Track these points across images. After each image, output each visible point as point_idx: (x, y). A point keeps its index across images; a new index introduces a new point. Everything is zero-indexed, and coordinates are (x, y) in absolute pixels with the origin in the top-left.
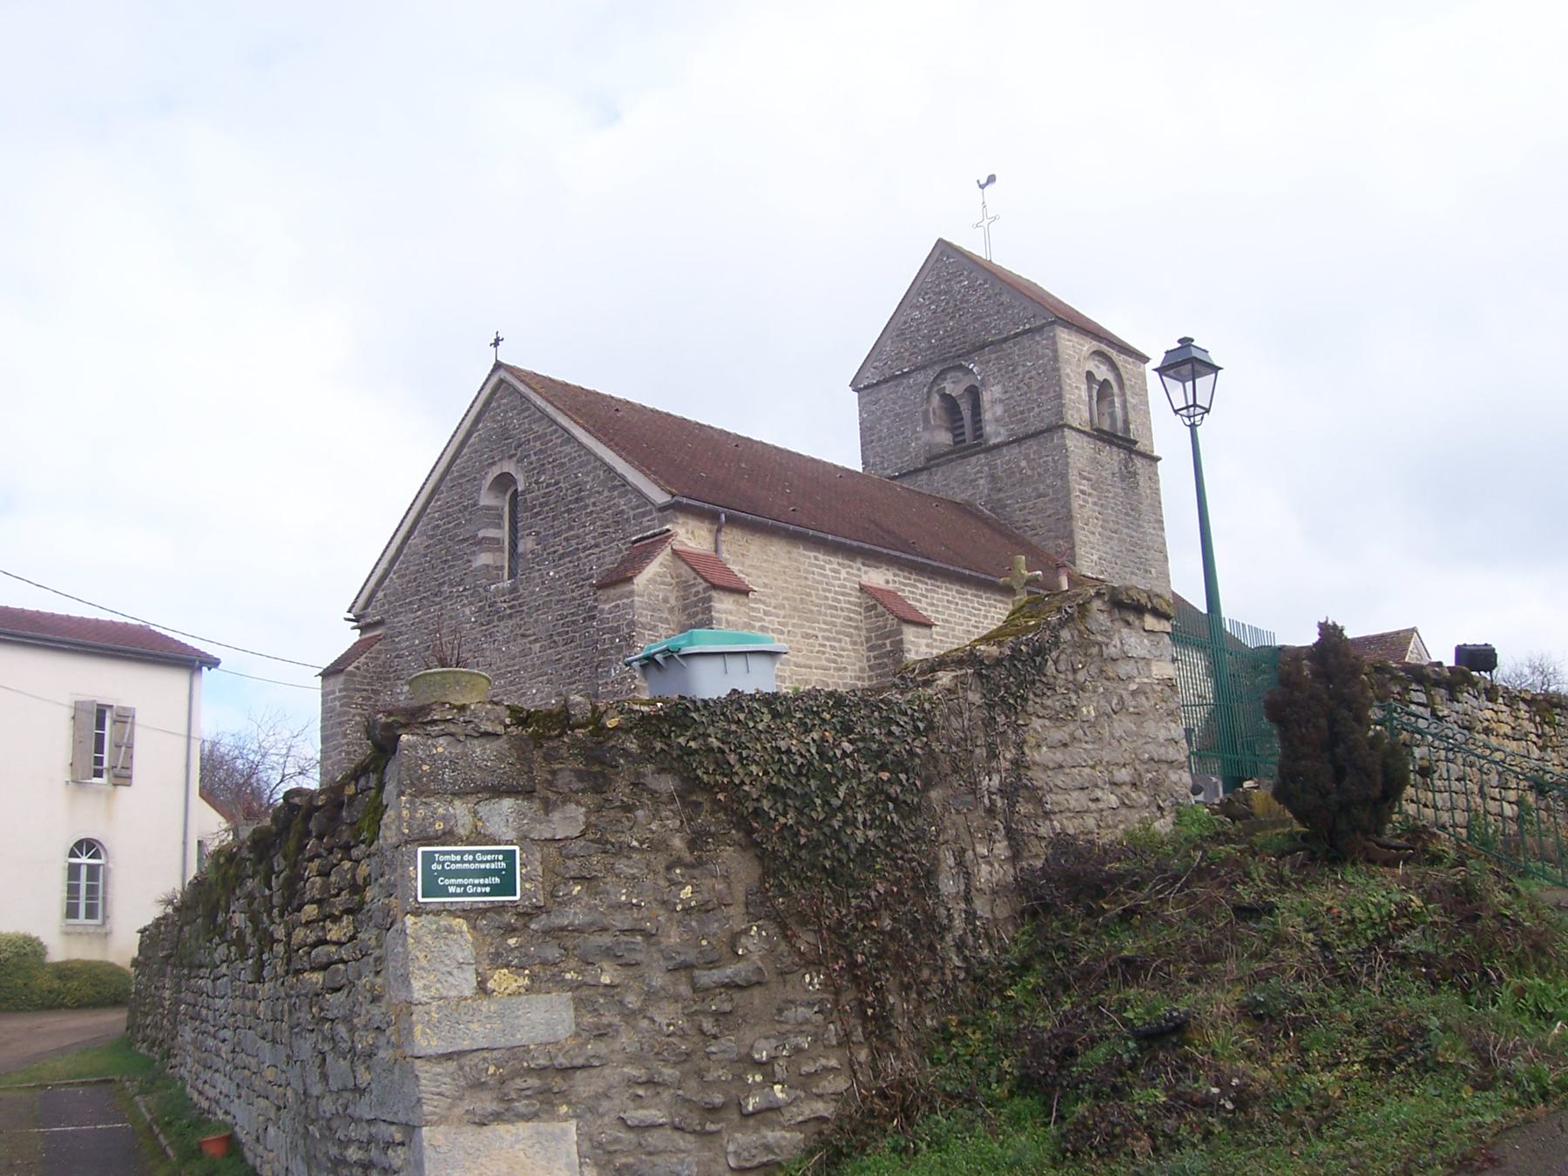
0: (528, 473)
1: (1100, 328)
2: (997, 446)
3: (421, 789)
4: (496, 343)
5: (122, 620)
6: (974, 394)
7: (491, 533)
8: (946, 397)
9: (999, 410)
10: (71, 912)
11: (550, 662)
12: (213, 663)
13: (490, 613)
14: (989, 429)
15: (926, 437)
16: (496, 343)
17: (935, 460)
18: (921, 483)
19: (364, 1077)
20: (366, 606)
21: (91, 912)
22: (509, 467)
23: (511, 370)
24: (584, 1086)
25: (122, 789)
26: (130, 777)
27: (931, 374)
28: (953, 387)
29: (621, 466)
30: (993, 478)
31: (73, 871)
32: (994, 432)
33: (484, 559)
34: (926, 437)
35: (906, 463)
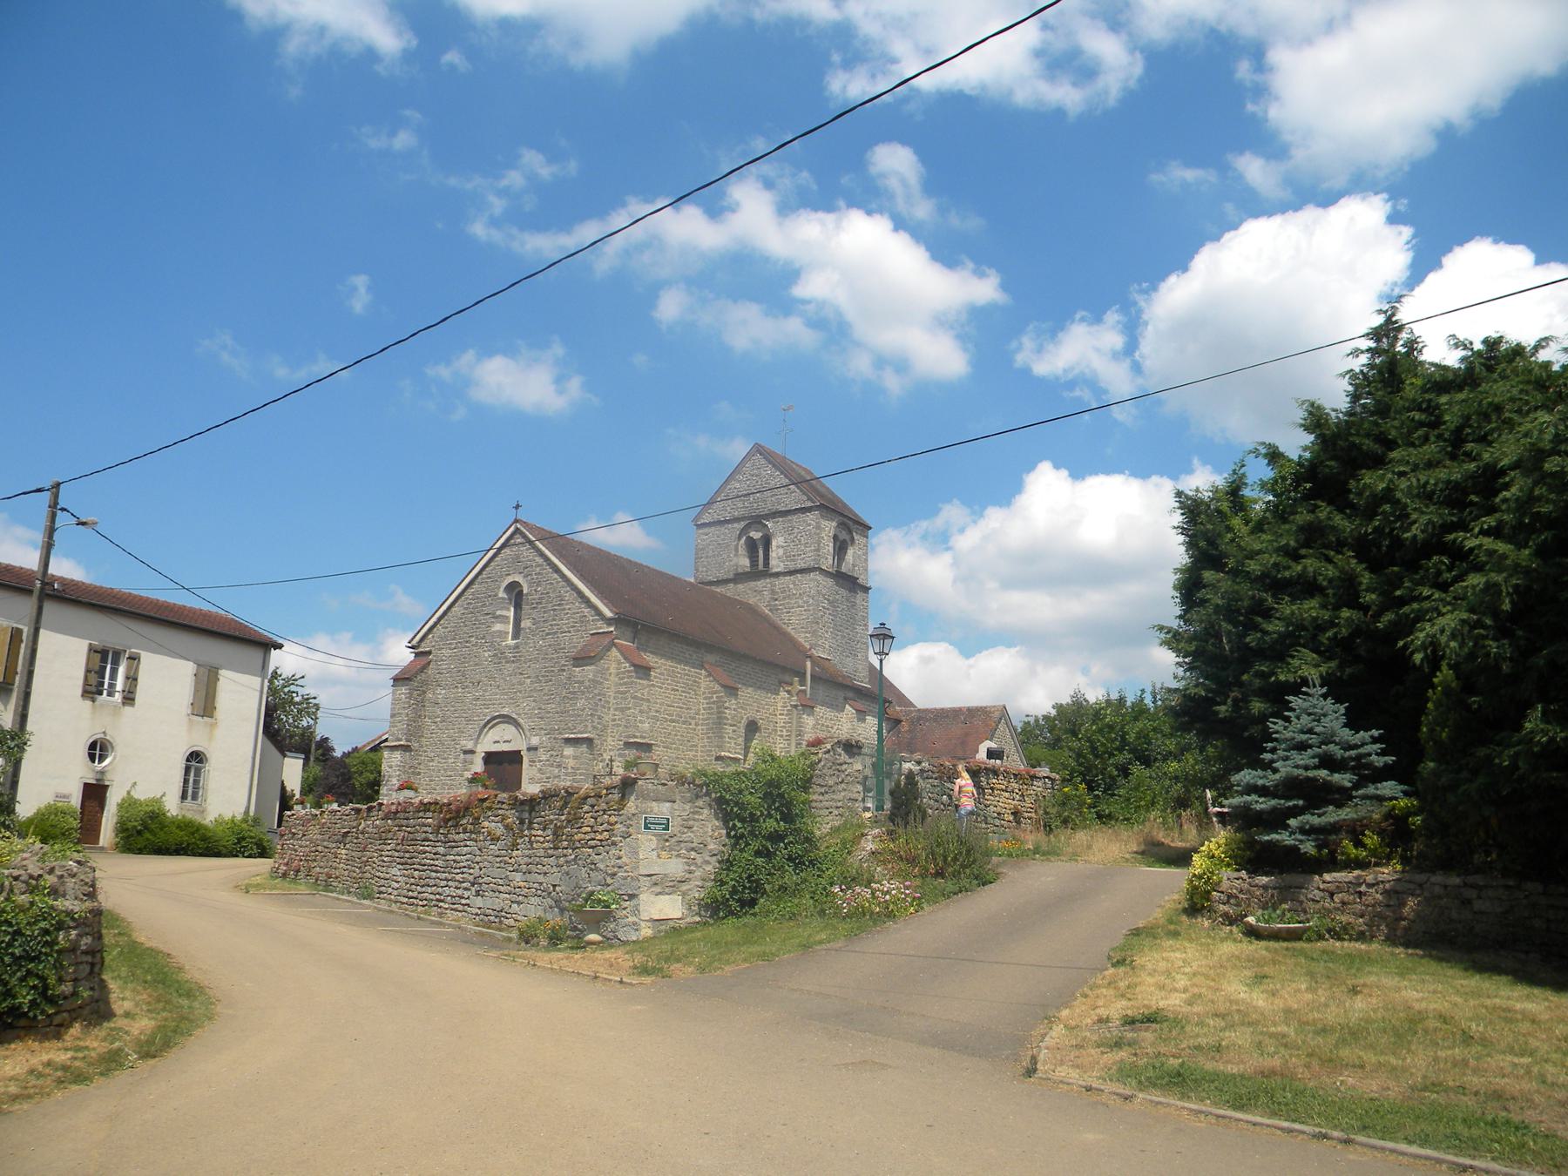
0: (530, 584)
1: (845, 505)
2: (777, 575)
3: (645, 797)
4: (517, 507)
5: (214, 609)
6: (767, 541)
7: (504, 613)
8: (750, 539)
9: (781, 551)
10: (184, 797)
11: (535, 690)
12: (280, 646)
13: (499, 656)
14: (773, 562)
15: (735, 560)
16: (517, 507)
17: (739, 578)
18: (729, 590)
19: (609, 881)
20: (422, 639)
21: (195, 797)
22: (519, 578)
23: (525, 524)
24: (684, 887)
25: (128, 709)
26: (133, 700)
27: (743, 524)
28: (756, 535)
29: (587, 592)
30: (773, 592)
31: (187, 769)
32: (776, 565)
33: (498, 627)
34: (735, 560)
35: (722, 575)
